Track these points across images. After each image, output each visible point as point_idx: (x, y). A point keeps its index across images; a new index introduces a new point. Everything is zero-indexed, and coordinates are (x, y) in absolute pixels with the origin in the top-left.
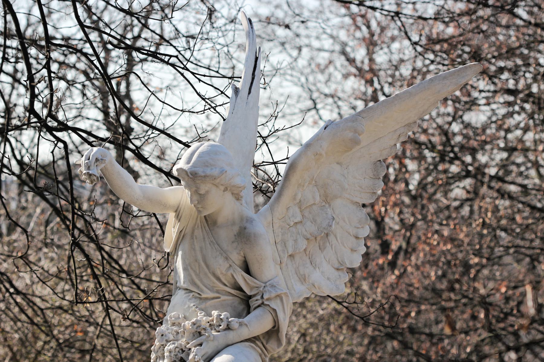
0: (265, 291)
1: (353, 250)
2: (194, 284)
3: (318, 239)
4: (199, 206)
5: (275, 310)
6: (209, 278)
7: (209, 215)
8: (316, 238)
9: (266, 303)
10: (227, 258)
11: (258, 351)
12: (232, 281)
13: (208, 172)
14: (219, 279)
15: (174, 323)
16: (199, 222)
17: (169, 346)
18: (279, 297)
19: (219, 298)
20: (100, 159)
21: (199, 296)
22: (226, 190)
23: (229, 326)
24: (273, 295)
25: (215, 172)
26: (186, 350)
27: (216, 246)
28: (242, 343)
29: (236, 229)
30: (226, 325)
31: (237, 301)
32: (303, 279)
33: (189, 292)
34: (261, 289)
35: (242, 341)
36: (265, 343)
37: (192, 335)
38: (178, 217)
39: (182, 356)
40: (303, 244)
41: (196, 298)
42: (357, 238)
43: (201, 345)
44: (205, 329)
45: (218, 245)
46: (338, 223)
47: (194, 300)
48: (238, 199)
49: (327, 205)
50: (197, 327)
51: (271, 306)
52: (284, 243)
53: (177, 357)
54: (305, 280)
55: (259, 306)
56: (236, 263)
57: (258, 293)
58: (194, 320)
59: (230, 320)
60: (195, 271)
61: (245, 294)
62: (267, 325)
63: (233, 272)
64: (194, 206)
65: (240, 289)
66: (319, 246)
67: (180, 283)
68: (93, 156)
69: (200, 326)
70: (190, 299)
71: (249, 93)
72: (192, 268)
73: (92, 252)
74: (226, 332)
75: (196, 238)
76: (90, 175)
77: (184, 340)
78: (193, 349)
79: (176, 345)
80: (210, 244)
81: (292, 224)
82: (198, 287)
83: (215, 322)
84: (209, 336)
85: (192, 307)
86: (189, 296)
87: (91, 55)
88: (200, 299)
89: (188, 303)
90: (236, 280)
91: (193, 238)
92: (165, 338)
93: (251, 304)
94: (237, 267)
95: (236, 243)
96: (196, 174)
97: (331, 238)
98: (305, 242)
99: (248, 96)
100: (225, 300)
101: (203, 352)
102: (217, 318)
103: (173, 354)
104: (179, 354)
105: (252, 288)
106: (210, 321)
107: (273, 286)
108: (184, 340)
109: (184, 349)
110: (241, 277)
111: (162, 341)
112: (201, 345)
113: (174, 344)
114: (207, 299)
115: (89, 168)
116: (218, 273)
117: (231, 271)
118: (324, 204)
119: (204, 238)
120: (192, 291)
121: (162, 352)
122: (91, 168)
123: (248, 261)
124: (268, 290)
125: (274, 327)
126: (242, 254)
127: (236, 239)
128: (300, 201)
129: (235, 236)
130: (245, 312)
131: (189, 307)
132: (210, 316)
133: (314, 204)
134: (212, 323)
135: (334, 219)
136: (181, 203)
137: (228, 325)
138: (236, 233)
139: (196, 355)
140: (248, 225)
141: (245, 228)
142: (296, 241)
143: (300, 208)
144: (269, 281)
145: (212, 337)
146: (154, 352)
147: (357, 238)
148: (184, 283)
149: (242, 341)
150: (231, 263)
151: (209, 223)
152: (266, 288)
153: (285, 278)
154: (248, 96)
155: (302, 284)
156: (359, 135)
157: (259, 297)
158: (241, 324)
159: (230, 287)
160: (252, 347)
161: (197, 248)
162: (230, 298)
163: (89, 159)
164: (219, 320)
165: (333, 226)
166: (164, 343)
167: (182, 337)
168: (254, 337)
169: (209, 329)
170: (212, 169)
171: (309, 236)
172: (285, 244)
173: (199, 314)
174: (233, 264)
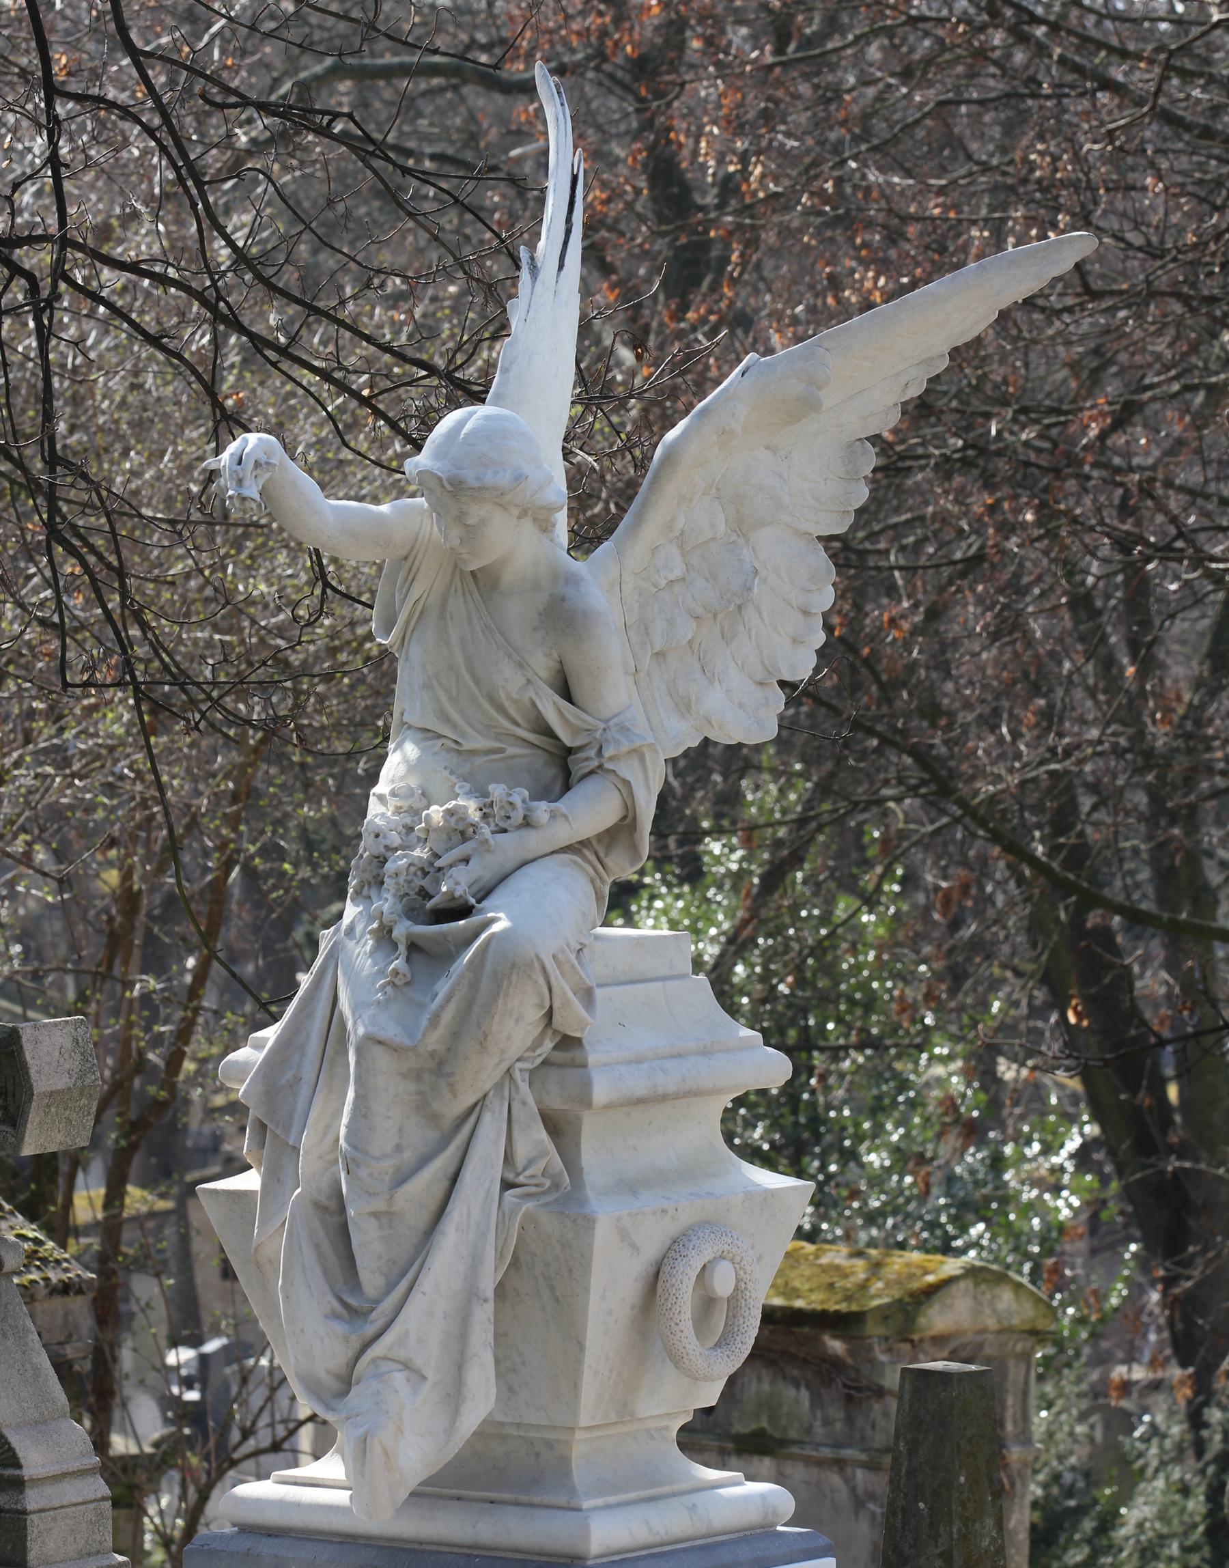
0: (607, 740)
1: (795, 641)
2: (446, 719)
3: (720, 616)
5: (627, 783)
8: (715, 617)
10: (521, 665)
11: (587, 873)
13: (489, 479)
14: (501, 709)
18: (637, 753)
22: (524, 513)
24: (624, 749)
25: (504, 479)
26: (432, 870)
27: (498, 636)
28: (555, 856)
31: (540, 760)
32: (684, 706)
34: (598, 735)
35: (552, 853)
36: (602, 855)
40: (686, 630)
41: (449, 750)
42: (806, 613)
46: (765, 580)
49: (741, 541)
52: (645, 628)
54: (689, 708)
55: (592, 772)
65: (549, 732)
66: (722, 632)
70: (436, 753)
71: (561, 267)
72: (441, 684)
74: (523, 832)
81: (663, 583)
82: (455, 727)
90: (539, 712)
97: (749, 612)
98: (693, 624)
100: (513, 757)
103: (401, 879)
105: (576, 731)
107: (624, 729)
110: (551, 707)
112: (466, 860)
114: (473, 753)
118: (734, 538)
119: (470, 619)
120: (440, 736)
122: (247, 483)
125: (624, 818)
126: (555, 655)
128: (682, 533)
130: (558, 787)
133: (714, 539)
135: (756, 572)
142: (670, 622)
143: (681, 547)
149: (552, 853)
153: (644, 705)
155: (683, 717)
156: (819, 388)
157: (592, 753)
158: (554, 815)
160: (575, 862)
162: (527, 751)
165: (756, 590)
168: (581, 843)
171: (699, 610)
172: (646, 628)
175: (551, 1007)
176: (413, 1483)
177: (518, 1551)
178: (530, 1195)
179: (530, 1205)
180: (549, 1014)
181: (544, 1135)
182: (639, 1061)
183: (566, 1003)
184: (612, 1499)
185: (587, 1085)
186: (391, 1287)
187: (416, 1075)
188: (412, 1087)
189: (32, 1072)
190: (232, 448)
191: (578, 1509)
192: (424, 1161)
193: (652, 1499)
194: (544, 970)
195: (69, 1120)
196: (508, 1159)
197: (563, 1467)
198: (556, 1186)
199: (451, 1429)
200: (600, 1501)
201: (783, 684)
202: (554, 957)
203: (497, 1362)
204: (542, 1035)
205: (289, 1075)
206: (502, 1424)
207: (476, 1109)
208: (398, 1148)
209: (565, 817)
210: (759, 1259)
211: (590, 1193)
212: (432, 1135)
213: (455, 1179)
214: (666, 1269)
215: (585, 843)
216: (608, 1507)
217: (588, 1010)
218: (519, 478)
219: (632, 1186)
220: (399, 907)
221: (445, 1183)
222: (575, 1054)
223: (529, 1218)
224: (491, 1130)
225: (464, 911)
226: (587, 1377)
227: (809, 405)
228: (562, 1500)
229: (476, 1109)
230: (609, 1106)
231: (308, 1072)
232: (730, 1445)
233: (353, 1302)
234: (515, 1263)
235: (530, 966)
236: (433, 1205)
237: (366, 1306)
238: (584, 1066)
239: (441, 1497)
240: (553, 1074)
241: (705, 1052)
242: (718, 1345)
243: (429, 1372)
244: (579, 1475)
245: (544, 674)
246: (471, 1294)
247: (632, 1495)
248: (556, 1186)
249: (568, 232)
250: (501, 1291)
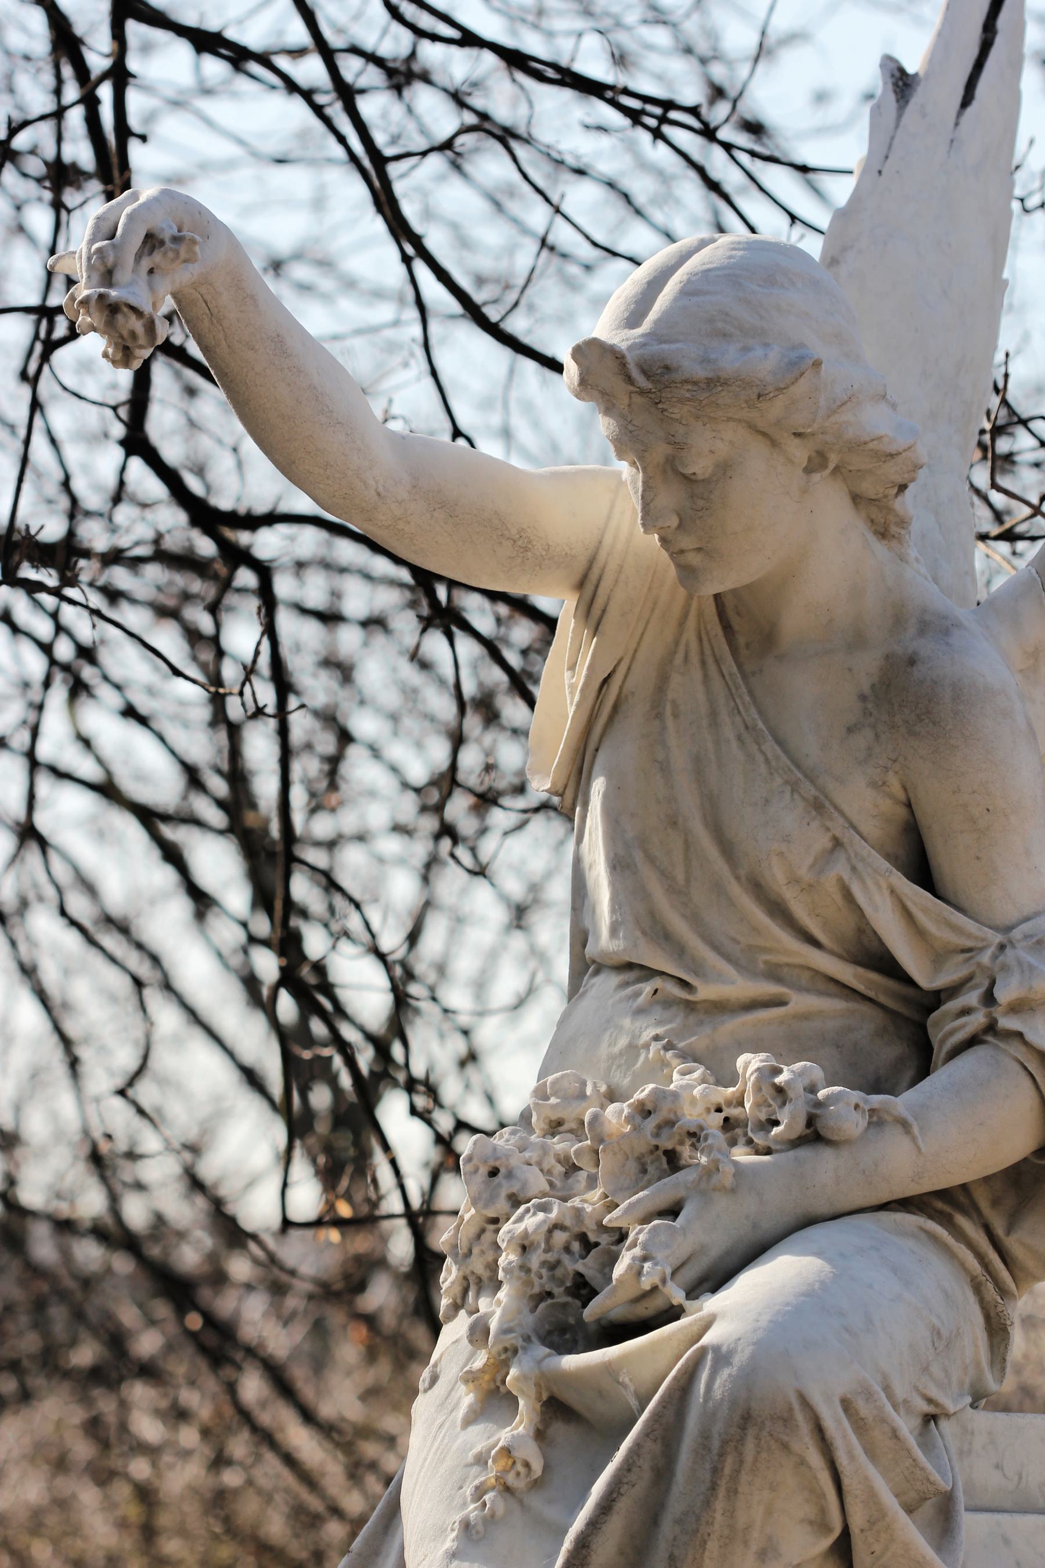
0: (1005, 968)
4: (687, 542)
6: (732, 903)
7: (734, 592)
9: (1006, 1023)
10: (819, 806)
11: (962, 1265)
12: (848, 924)
14: (779, 911)
15: (560, 1123)
16: (690, 635)
17: (520, 1219)
19: (779, 1002)
20: (166, 236)
21: (682, 994)
22: (817, 463)
23: (819, 1125)
26: (604, 1240)
27: (770, 746)
30: (802, 1121)
33: (639, 980)
34: (985, 958)
36: (1000, 1231)
37: (632, 1166)
39: (580, 1266)
41: (669, 1003)
43: (673, 1212)
44: (695, 1136)
45: (780, 742)
47: (658, 1013)
48: (883, 534)
50: (659, 1127)
51: (1029, 1036)
53: (559, 1272)
55: (972, 1042)
56: (864, 828)
57: (969, 978)
58: (642, 1094)
59: (822, 1094)
60: (665, 875)
61: (909, 991)
63: (846, 876)
64: (664, 540)
67: (598, 938)
68: (131, 217)
69: (670, 1123)
71: (967, 99)
72: (651, 859)
74: (804, 1153)
75: (676, 715)
76: (111, 310)
77: (596, 1194)
78: (639, 1234)
79: (554, 1215)
80: (739, 738)
82: (679, 951)
83: (747, 1105)
84: (713, 1169)
85: (647, 1046)
86: (637, 994)
87: (298, 53)
88: (690, 1007)
89: (627, 1022)
91: (659, 716)
92: (506, 1188)
93: (936, 1037)
94: (865, 849)
95: (868, 733)
96: (667, 368)
99: (959, 114)
100: (805, 1017)
101: (683, 1247)
102: (758, 1089)
103: (535, 1260)
104: (566, 1259)
105: (939, 957)
106: (729, 1104)
108: (596, 1194)
109: (592, 1238)
111: (491, 1200)
113: (545, 1208)
114: (720, 1008)
115: (108, 276)
116: (777, 877)
117: (840, 868)
119: (713, 715)
120: (649, 973)
121: (490, 1257)
122: (123, 276)
123: (923, 820)
124: (1020, 963)
126: (896, 788)
127: (867, 713)
129: (863, 698)
130: (909, 1074)
131: (633, 1049)
132: (731, 1079)
134: (734, 1112)
136: (608, 540)
137: (811, 1121)
138: (866, 689)
139: (645, 1259)
140: (925, 647)
141: (912, 661)
144: (1027, 919)
145: (728, 1170)
146: (455, 1256)
148: (614, 931)
150: (838, 827)
151: (741, 640)
152: (1009, 951)
154: (959, 114)
158: (876, 1120)
159: (832, 953)
160: (933, 1237)
161: (680, 759)
163: (112, 236)
164: (767, 1092)
167: (592, 1182)
168: (943, 1194)
169: (717, 1137)
170: (746, 349)
173: (676, 1076)
174: (848, 836)
175: (846, 1534)
183: (878, 1517)
194: (819, 1430)
202: (846, 1404)
209: (904, 1124)
217: (939, 1549)
220: (529, 1320)
235: (787, 1420)
245: (871, 827)
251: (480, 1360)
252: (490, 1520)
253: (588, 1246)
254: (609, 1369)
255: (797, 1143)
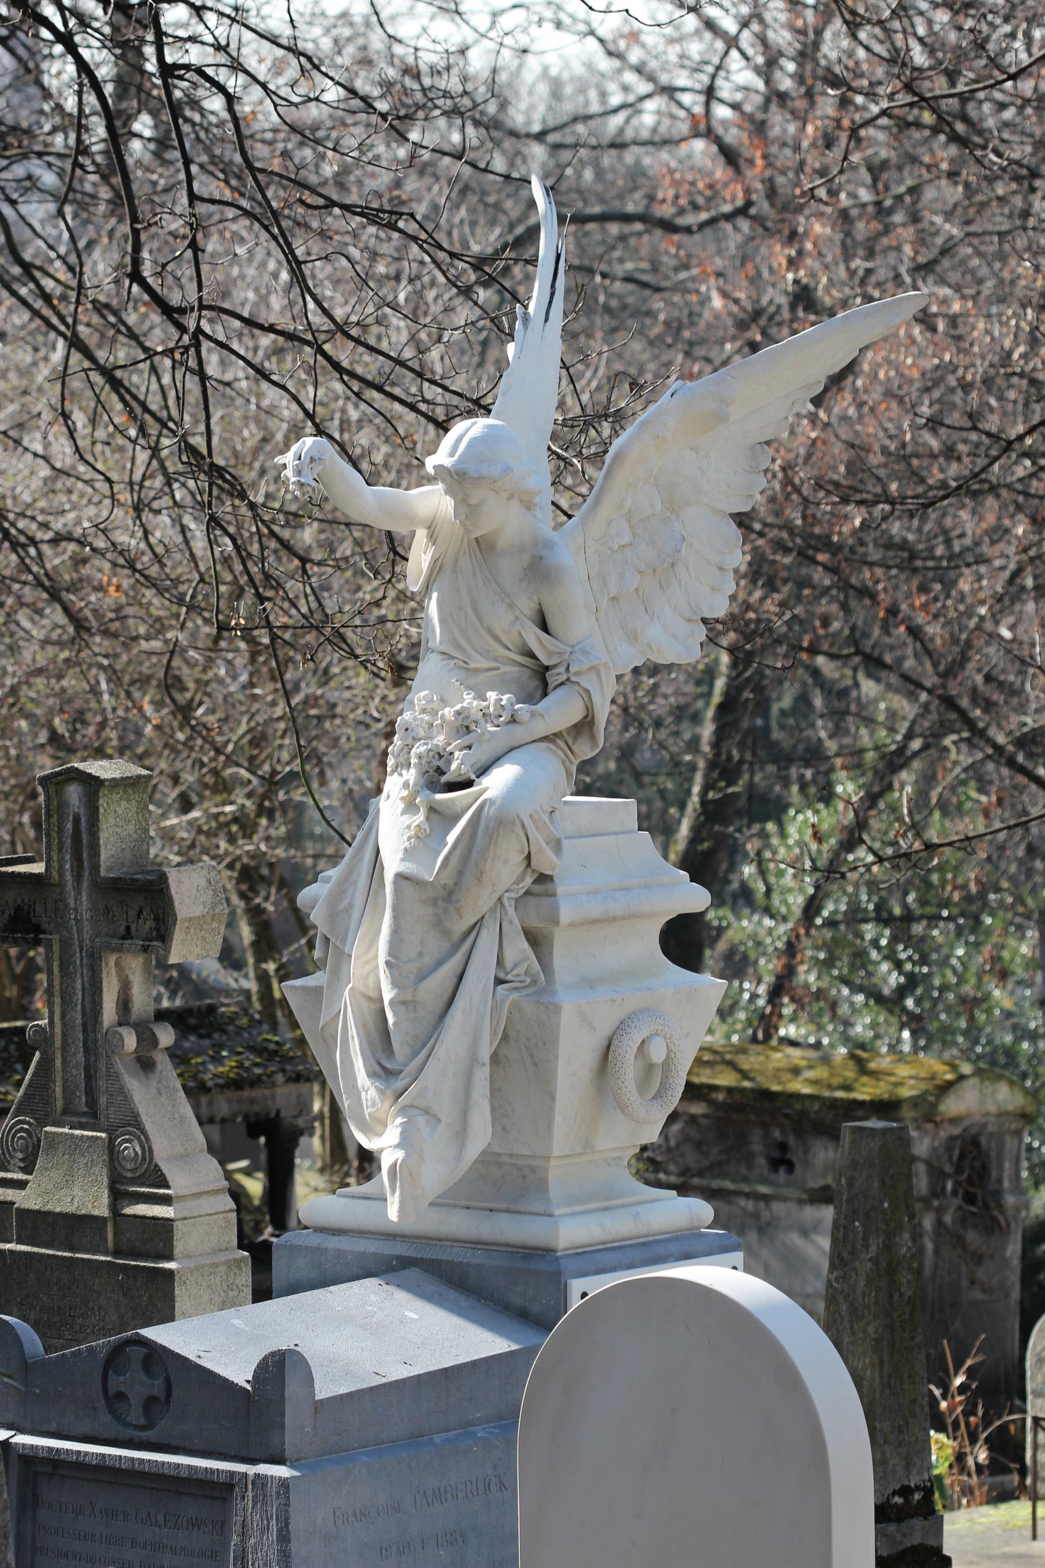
1: (714, 589)
2: (458, 646)
5: (587, 691)
10: (511, 606)
18: (595, 669)
22: (511, 497)
24: (585, 666)
29: (526, 558)
31: (527, 673)
32: (632, 637)
38: (432, 538)
42: (721, 569)
48: (529, 508)
58: (458, 707)
62: (576, 715)
65: (531, 655)
73: (79, 425)
78: (457, 754)
81: (616, 547)
82: (463, 651)
92: (411, 734)
105: (550, 654)
107: (585, 652)
108: (441, 738)
112: (470, 747)
114: (477, 670)
116: (497, 629)
117: (518, 627)
130: (538, 695)
132: (485, 699)
147: (721, 569)
162: (516, 669)
166: (410, 741)
176: (431, 1196)
177: (508, 1245)
178: (516, 989)
179: (515, 995)
180: (528, 857)
181: (526, 945)
182: (596, 892)
184: (577, 1209)
185: (555, 910)
186: (415, 1054)
187: (434, 902)
188: (430, 911)
189: (176, 903)
190: (294, 448)
191: (551, 1215)
192: (439, 964)
193: (606, 1209)
195: (204, 939)
196: (500, 962)
197: (543, 1184)
198: (534, 982)
199: (459, 1157)
200: (568, 1210)
201: (704, 621)
203: (493, 1109)
204: (524, 873)
205: (346, 902)
206: (499, 1155)
207: (476, 927)
208: (420, 955)
210: (687, 1036)
211: (558, 987)
212: (445, 945)
213: (461, 977)
214: (615, 1042)
215: (558, 735)
216: (574, 1214)
218: (507, 470)
219: (590, 983)
221: (455, 980)
222: (548, 886)
223: (516, 1006)
224: (487, 940)
225: (468, 784)
226: (558, 1120)
227: (720, 418)
228: (540, 1208)
229: (476, 927)
230: (572, 925)
231: (359, 901)
232: (805, 1197)
233: (388, 1065)
234: (505, 1037)
235: (513, 822)
236: (446, 996)
237: (398, 1067)
238: (554, 895)
239: (455, 1206)
240: (532, 900)
241: (646, 886)
242: (654, 1098)
243: (443, 1117)
244: (552, 1193)
245: (528, 613)
246: (473, 1060)
247: (592, 1206)
248: (534, 982)
249: (552, 294)
250: (495, 1058)
251: (405, 793)
252: (413, 848)
253: (441, 757)
254: (451, 800)
255: (508, 723)
